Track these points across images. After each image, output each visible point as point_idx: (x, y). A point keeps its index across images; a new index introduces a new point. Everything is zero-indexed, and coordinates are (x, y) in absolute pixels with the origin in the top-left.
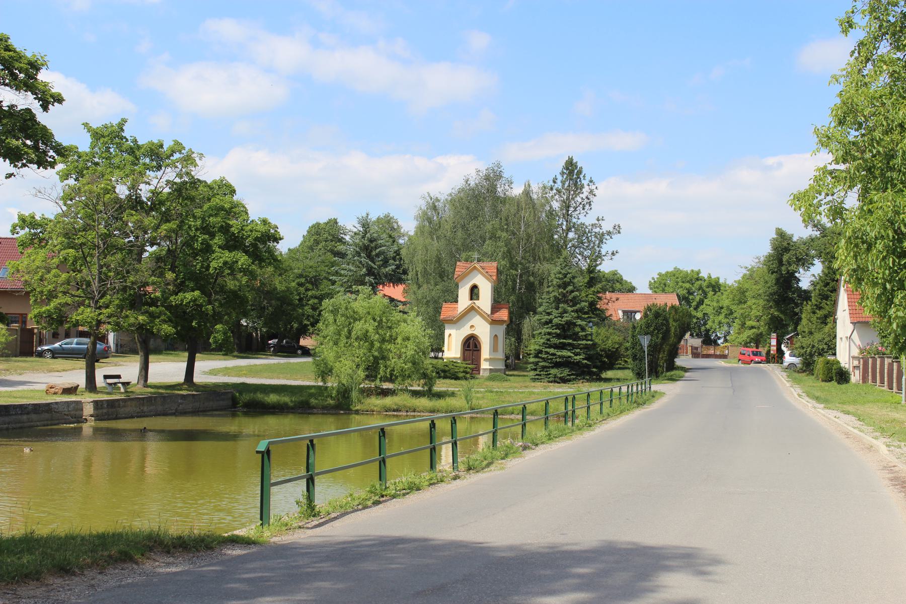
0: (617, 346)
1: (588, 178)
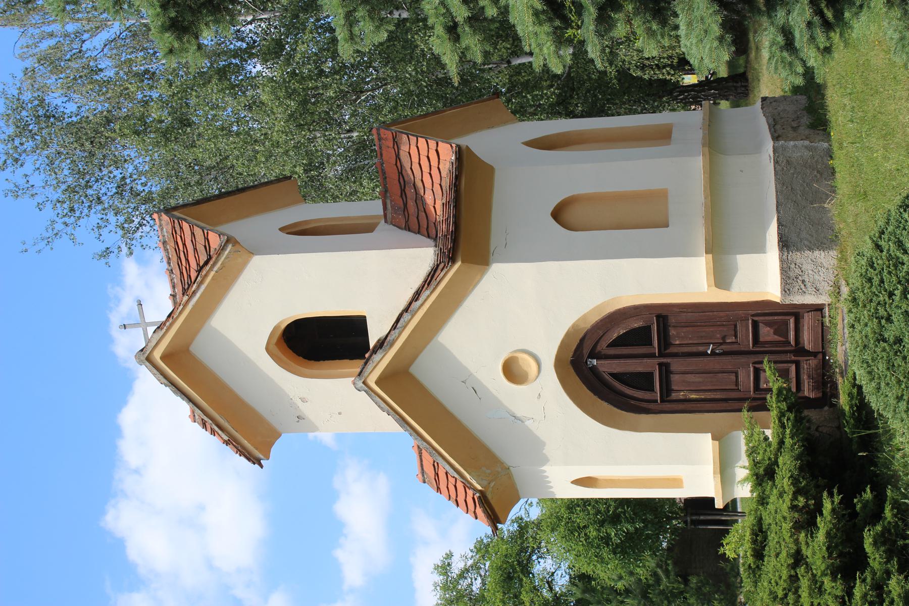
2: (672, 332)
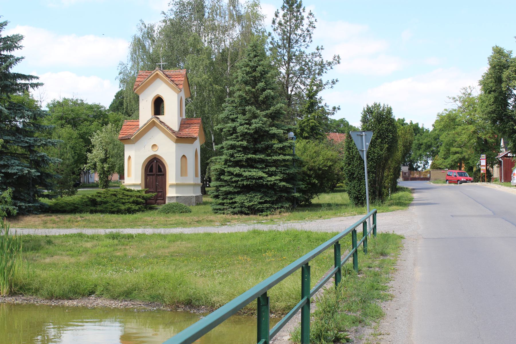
0: (329, 163)
1: (307, 11)
2: (161, 176)
